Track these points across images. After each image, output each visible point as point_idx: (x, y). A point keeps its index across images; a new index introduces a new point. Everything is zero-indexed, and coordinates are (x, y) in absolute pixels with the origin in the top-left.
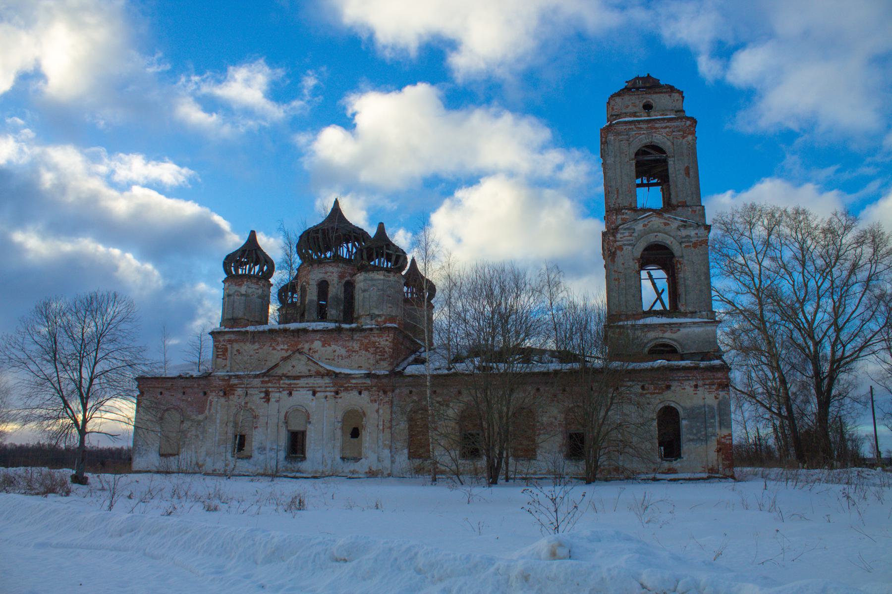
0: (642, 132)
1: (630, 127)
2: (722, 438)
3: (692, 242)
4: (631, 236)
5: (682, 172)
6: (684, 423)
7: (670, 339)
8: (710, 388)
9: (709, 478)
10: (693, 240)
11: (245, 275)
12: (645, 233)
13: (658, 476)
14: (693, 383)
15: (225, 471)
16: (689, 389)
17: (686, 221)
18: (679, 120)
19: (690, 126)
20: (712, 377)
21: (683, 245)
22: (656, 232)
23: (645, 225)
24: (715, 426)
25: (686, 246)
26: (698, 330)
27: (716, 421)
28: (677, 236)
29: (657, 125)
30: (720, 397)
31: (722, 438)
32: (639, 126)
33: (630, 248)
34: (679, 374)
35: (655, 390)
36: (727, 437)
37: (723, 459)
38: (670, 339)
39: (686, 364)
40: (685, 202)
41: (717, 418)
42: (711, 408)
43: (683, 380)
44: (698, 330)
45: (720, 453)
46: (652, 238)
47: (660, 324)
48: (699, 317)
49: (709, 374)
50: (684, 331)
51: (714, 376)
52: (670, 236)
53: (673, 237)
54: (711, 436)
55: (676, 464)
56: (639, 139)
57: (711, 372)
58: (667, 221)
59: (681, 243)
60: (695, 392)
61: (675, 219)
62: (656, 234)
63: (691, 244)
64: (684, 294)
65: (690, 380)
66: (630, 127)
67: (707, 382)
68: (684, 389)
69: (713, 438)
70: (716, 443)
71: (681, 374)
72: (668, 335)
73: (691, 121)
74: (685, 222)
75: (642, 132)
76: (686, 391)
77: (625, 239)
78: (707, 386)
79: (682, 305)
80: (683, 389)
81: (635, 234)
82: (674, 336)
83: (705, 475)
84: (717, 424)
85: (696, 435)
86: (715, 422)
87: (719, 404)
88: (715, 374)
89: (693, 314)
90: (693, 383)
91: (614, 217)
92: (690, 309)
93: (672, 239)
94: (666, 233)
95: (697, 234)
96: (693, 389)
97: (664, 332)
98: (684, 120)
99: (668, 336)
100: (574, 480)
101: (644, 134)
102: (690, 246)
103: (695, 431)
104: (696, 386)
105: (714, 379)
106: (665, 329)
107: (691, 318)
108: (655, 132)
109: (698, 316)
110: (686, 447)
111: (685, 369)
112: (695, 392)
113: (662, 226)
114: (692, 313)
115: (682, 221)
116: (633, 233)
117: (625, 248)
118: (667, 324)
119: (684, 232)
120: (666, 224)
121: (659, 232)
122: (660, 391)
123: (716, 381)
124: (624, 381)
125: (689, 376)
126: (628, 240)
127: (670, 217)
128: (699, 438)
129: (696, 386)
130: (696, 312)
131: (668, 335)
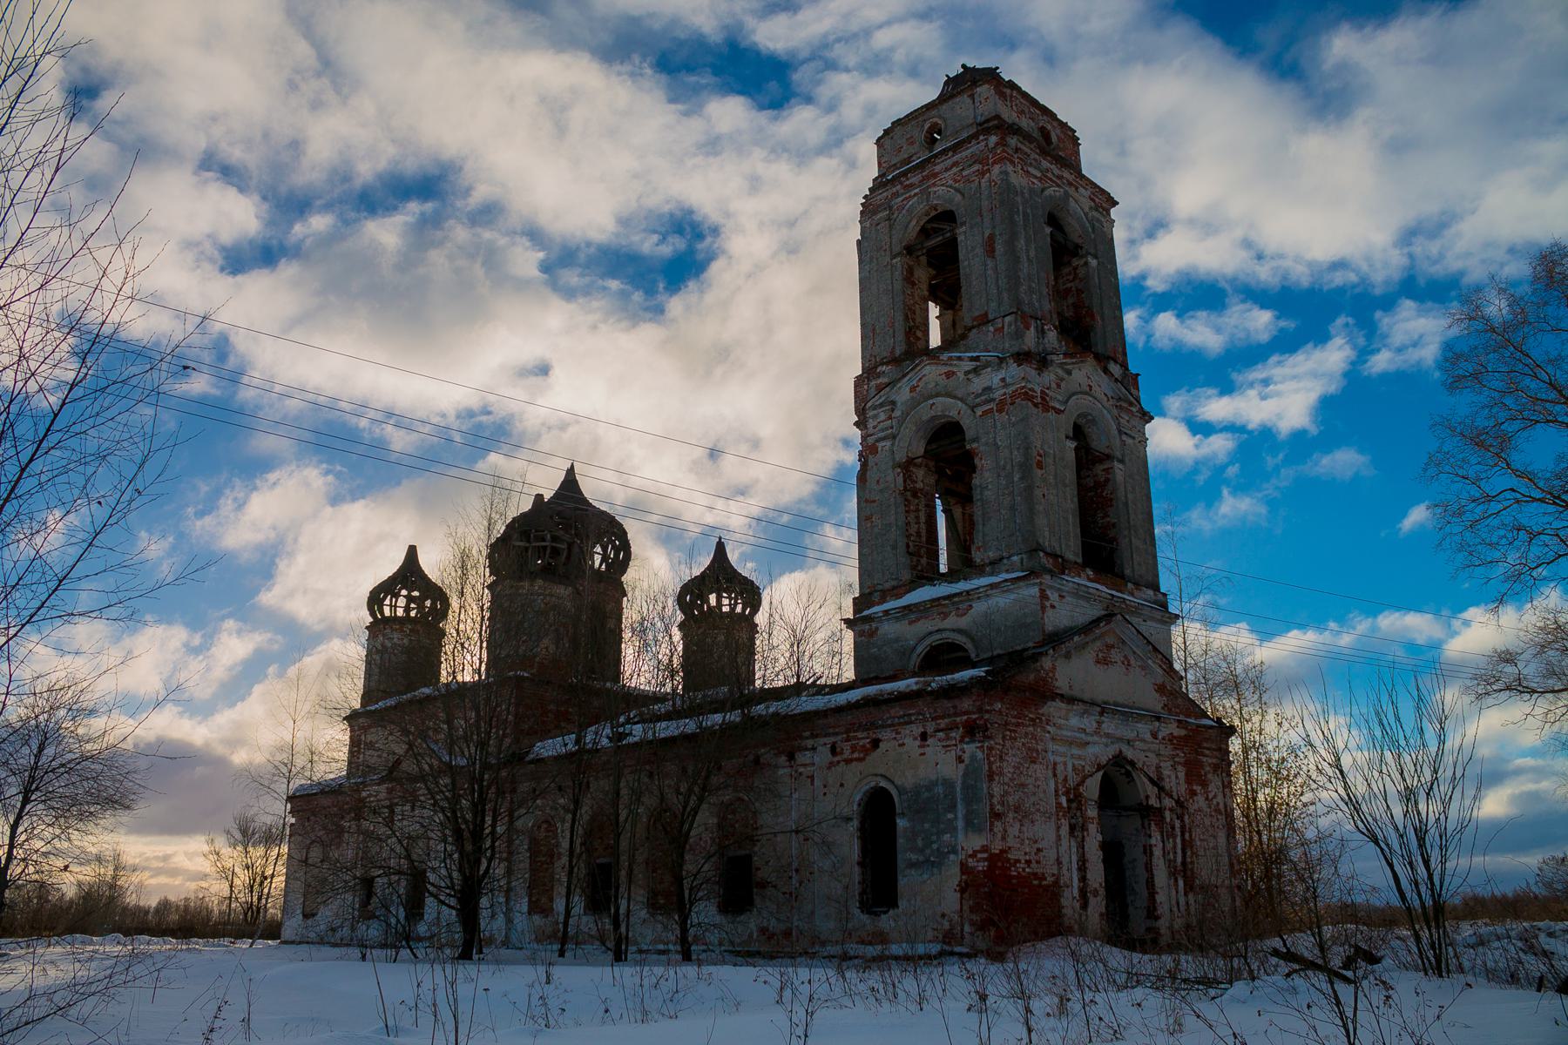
0: (912, 193)
1: (894, 190)
2: (970, 856)
3: (993, 400)
4: (890, 418)
5: (979, 250)
6: (901, 823)
7: (954, 630)
8: (948, 738)
9: (941, 954)
10: (997, 395)
11: (395, 619)
12: (914, 404)
13: (853, 948)
14: (917, 730)
15: (352, 940)
16: (912, 745)
17: (978, 357)
18: (974, 142)
19: (997, 144)
20: (952, 711)
21: (979, 412)
22: (931, 397)
23: (913, 389)
24: (955, 829)
25: (985, 413)
26: (1001, 601)
27: (960, 815)
28: (968, 394)
29: (937, 168)
30: (966, 757)
31: (970, 856)
32: (908, 182)
33: (888, 444)
34: (893, 712)
35: (853, 752)
36: (979, 856)
37: (972, 910)
38: (954, 630)
39: (908, 686)
40: (986, 314)
41: (961, 810)
42: (948, 784)
43: (900, 724)
44: (1001, 601)
45: (966, 895)
46: (925, 412)
47: (933, 600)
48: (1007, 571)
49: (948, 704)
50: (979, 607)
51: (955, 707)
52: (955, 397)
53: (961, 400)
54: (949, 852)
55: (886, 922)
56: (908, 211)
57: (950, 698)
58: (950, 369)
59: (973, 408)
60: (922, 751)
61: (959, 358)
62: (931, 402)
63: (992, 405)
64: (981, 522)
65: (911, 722)
66: (894, 190)
67: (943, 723)
68: (904, 744)
69: (952, 857)
70: (956, 870)
71: (897, 711)
72: (952, 621)
73: (995, 134)
74: (977, 359)
75: (912, 193)
76: (905, 748)
77: (879, 427)
78: (941, 735)
79: (979, 548)
80: (900, 745)
81: (897, 413)
82: (963, 622)
83: (935, 948)
84: (960, 824)
85: (921, 851)
86: (956, 818)
87: (965, 775)
88: (957, 702)
89: (995, 564)
90: (917, 730)
91: (866, 387)
92: (992, 554)
93: (960, 404)
94: (948, 395)
95: (1003, 380)
96: (918, 743)
97: (945, 616)
98: (981, 138)
99: (952, 624)
100: (728, 957)
101: (915, 195)
102: (991, 410)
103: (920, 843)
104: (924, 736)
105: (956, 715)
106: (944, 610)
107: (992, 574)
108: (934, 185)
109: (1004, 568)
110: (905, 880)
111: (902, 697)
112: (922, 751)
113: (942, 381)
114: (993, 563)
115: (972, 359)
116: (893, 410)
117: (880, 445)
118: (945, 598)
119: (978, 383)
120: (949, 375)
121: (938, 395)
122: (862, 755)
123: (958, 719)
124: (801, 738)
125: (910, 715)
126: (882, 430)
127: (950, 358)
128: (927, 861)
129: (924, 736)
130: (1001, 559)
131: (952, 621)
